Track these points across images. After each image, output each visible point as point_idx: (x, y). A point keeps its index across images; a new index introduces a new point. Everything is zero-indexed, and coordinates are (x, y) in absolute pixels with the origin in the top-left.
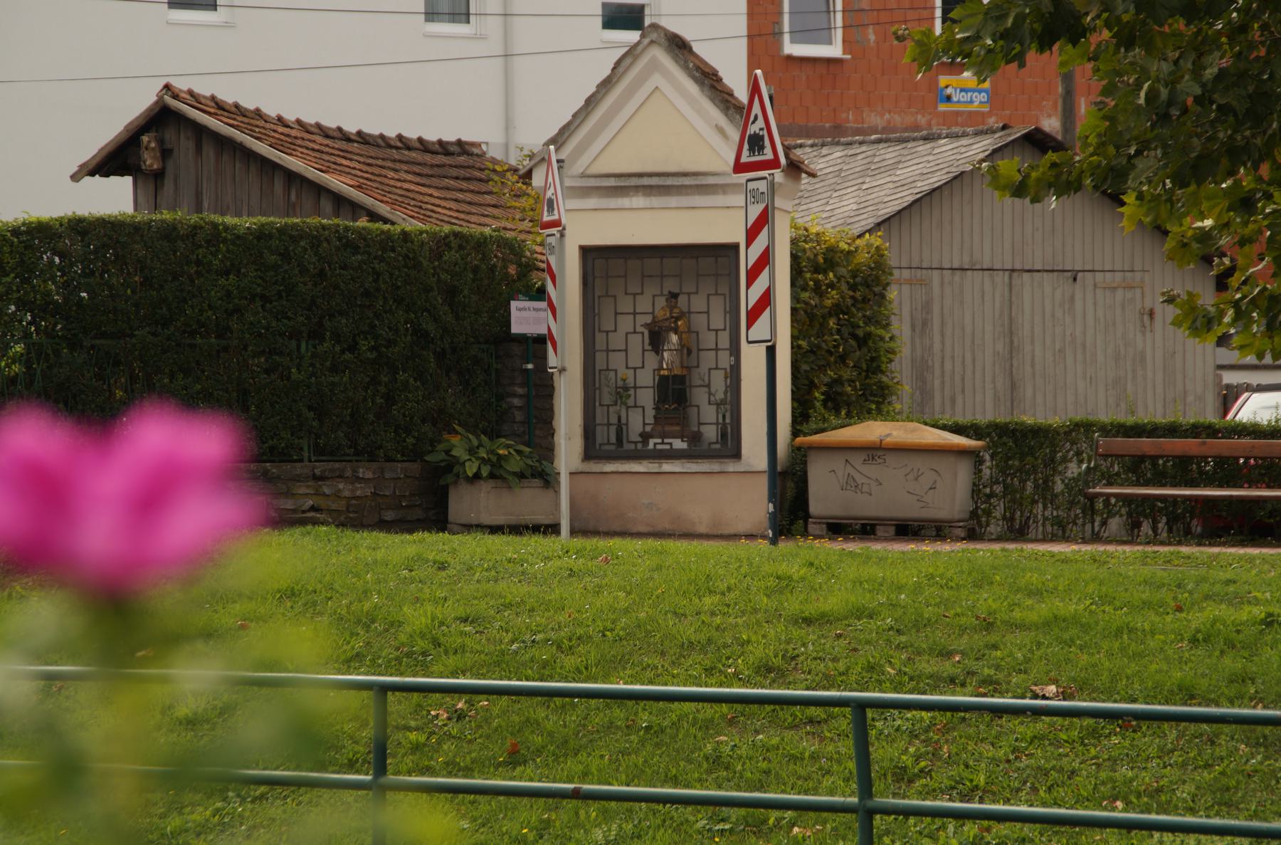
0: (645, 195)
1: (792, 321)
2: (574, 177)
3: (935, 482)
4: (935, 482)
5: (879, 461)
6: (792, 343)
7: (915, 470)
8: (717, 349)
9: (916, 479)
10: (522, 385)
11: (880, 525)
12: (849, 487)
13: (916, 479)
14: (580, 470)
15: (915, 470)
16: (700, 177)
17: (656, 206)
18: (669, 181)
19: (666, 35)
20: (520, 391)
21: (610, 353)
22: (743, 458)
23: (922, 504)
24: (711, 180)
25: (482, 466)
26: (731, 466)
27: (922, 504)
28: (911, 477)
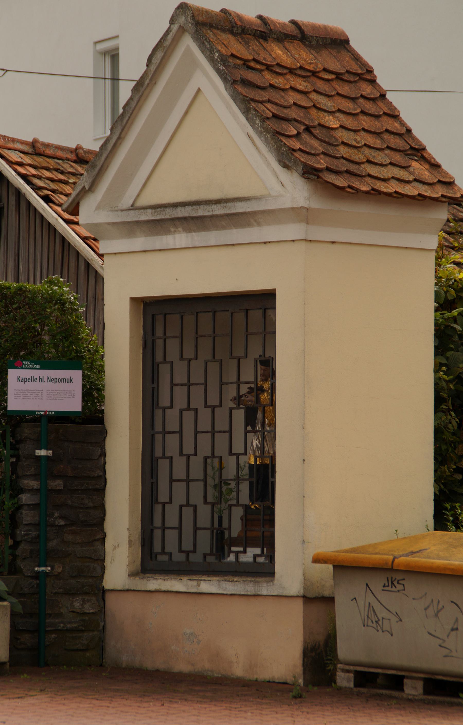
0: (188, 230)
1: (82, 401)
2: (122, 211)
3: (457, 620)
4: (457, 620)
5: (399, 587)
6: (275, 428)
7: (435, 603)
8: (213, 432)
9: (436, 615)
10: (36, 477)
11: (408, 677)
12: (370, 623)
13: (436, 615)
14: (127, 587)
15: (435, 603)
16: (229, 204)
17: (197, 244)
18: (202, 211)
19: (193, 17)
20: (34, 484)
21: (167, 435)
22: (277, 576)
23: (446, 652)
24: (240, 208)
25: (397, 538)
26: (265, 589)
27: (446, 652)
28: (431, 612)
